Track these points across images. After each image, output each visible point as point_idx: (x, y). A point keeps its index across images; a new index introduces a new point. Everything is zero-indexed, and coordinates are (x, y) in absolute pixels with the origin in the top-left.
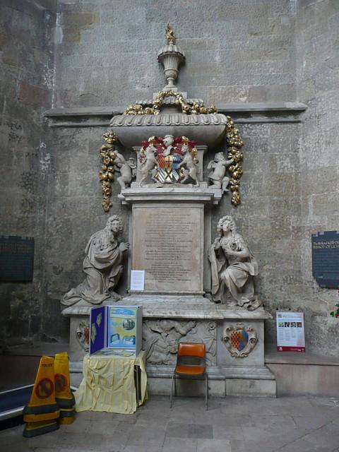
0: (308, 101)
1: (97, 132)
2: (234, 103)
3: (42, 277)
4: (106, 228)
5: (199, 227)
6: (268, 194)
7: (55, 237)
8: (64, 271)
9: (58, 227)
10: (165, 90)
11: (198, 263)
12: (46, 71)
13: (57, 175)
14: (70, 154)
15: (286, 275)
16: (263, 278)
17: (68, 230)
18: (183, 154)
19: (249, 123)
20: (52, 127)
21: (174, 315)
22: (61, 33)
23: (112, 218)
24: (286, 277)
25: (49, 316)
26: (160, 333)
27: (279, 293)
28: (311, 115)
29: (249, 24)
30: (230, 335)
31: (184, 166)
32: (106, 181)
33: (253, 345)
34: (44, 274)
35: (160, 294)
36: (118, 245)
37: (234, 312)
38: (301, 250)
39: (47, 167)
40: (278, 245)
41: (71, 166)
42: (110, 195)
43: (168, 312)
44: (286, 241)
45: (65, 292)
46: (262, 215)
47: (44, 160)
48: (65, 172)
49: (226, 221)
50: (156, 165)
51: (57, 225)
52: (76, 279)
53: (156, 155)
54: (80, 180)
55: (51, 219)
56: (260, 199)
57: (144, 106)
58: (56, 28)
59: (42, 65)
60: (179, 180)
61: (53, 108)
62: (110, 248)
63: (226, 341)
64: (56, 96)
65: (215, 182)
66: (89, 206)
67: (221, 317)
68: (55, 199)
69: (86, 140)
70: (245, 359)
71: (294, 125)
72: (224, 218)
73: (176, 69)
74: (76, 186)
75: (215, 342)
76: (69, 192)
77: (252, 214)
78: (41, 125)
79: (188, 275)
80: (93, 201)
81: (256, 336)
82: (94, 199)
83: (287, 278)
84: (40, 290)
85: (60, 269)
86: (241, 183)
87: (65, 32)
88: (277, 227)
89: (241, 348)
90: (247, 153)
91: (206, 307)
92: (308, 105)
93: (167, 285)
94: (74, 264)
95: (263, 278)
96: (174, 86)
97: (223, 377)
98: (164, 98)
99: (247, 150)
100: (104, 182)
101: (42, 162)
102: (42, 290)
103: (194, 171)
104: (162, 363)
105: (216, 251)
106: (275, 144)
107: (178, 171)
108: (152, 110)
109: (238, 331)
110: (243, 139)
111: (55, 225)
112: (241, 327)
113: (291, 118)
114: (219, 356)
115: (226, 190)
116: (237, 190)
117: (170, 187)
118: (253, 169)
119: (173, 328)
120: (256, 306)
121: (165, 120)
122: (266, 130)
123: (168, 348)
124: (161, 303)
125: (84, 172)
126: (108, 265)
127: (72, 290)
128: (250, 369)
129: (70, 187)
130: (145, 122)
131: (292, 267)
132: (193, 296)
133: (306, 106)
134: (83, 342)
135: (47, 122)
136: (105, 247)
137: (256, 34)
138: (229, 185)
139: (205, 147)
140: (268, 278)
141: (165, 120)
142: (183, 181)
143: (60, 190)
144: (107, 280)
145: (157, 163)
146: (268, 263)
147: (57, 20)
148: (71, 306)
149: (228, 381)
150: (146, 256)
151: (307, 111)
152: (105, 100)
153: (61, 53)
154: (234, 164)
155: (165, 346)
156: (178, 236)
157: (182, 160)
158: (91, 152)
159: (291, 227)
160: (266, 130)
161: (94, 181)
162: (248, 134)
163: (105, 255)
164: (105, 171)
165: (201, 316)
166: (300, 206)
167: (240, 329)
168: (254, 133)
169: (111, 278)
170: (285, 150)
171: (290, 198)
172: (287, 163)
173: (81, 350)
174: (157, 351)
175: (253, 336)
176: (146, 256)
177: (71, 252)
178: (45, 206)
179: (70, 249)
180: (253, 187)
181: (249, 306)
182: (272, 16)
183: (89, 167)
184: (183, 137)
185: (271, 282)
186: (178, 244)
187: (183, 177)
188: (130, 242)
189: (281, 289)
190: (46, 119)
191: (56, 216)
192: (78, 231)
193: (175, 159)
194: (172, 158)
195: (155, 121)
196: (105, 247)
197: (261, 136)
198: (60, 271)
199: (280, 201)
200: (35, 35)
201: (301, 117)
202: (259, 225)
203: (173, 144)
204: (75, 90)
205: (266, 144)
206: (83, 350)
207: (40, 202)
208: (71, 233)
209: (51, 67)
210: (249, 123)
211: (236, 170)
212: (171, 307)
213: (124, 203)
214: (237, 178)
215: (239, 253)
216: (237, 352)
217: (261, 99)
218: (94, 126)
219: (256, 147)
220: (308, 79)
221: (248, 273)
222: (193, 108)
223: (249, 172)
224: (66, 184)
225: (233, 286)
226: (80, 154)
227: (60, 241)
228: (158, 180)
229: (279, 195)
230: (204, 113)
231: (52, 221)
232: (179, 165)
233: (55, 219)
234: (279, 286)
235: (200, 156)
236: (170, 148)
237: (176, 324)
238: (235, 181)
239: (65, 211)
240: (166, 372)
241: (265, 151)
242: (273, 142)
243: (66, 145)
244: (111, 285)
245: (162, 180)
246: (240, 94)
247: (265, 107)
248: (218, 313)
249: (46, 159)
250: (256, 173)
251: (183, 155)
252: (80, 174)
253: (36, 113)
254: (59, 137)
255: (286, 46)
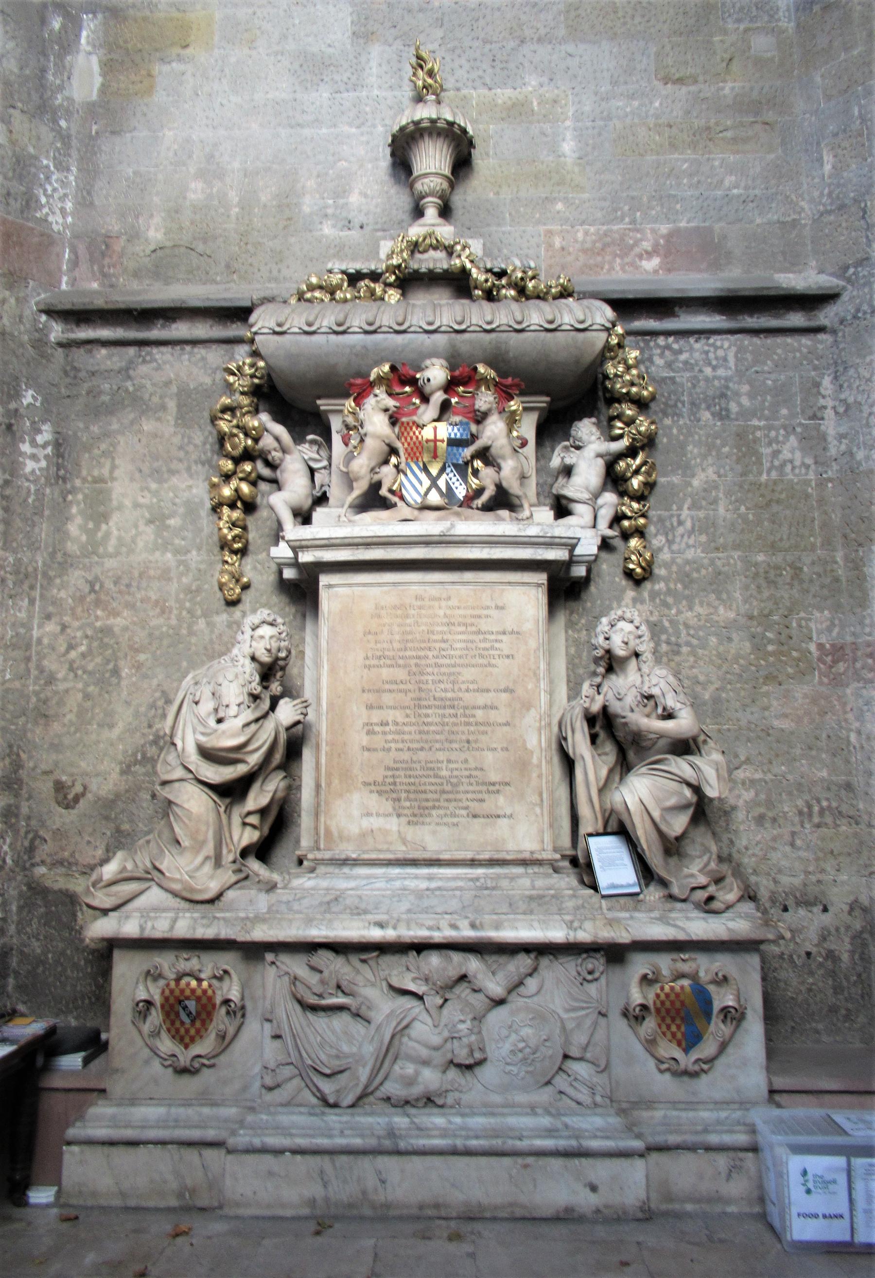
0: (847, 268)
1: (203, 359)
2: (622, 276)
3: (17, 816)
4: (235, 651)
5: (533, 644)
6: (736, 547)
7: (61, 687)
8: (89, 796)
9: (73, 654)
10: (416, 231)
11: (535, 761)
12: (48, 178)
13: (73, 491)
14: (115, 426)
15: (807, 797)
16: (734, 808)
17: (108, 661)
18: (480, 418)
19: (667, 333)
20: (61, 345)
21: (467, 933)
22: (96, 68)
23: (255, 619)
24: (807, 802)
25: (36, 947)
26: (420, 998)
27: (785, 856)
28: (858, 310)
29: (658, 54)
30: (651, 996)
31: (484, 454)
32: (232, 506)
33: (725, 1030)
34: (24, 810)
35: (414, 863)
36: (273, 707)
37: (663, 920)
38: (850, 716)
39: (44, 464)
40: (775, 703)
41: (117, 462)
42: (243, 552)
43: (444, 924)
44: (801, 692)
45: (92, 868)
46: (721, 610)
47: (33, 443)
48: (100, 480)
49: (622, 624)
50: (393, 451)
51: (71, 647)
52: (131, 821)
53: (394, 421)
54: (149, 507)
55: (51, 627)
56: (712, 562)
57: (354, 278)
58: (81, 58)
59: (36, 158)
60: (468, 501)
61: (64, 287)
62: (248, 715)
63: (639, 1019)
64: (74, 251)
65: (578, 508)
66: (174, 586)
67: (623, 937)
68: (66, 564)
69: (168, 383)
70: (704, 1078)
71: (806, 341)
72: (613, 615)
73: (447, 171)
74: (136, 526)
75: (602, 1021)
76: (113, 542)
77: (691, 609)
78: (26, 338)
79: (501, 800)
80: (188, 569)
81: (738, 999)
82: (193, 566)
83: (810, 807)
84: (9, 861)
85: (78, 789)
86: (651, 513)
87: (109, 67)
88: (770, 648)
89: (691, 1041)
90: (668, 422)
91: (570, 904)
92: (849, 280)
93: (434, 833)
94: (123, 772)
95: (734, 808)
96: (440, 221)
97: (637, 1144)
98: (413, 252)
99: (665, 414)
100: (226, 510)
101: (26, 448)
102: (16, 862)
103: (515, 469)
104: (429, 1101)
105: (591, 720)
106: (752, 396)
107: (462, 469)
108: (378, 288)
109: (677, 985)
110: (653, 380)
111: (63, 649)
112: (686, 968)
113: (796, 319)
114: (618, 1070)
115: (610, 533)
116: (640, 532)
117: (439, 519)
118: (687, 470)
119: (463, 978)
120: (731, 897)
121: (418, 319)
122: (720, 353)
123: (448, 1045)
124: (419, 895)
125: (161, 481)
126: (241, 769)
127: (120, 855)
128: (723, 1114)
129: (115, 526)
130: (357, 321)
131: (824, 774)
132: (520, 870)
133: (842, 283)
134: (155, 1034)
135: (46, 328)
136: (233, 710)
137: (680, 81)
138: (617, 519)
139: (542, 401)
140: (751, 805)
141: (418, 319)
142: (479, 502)
143: (84, 538)
144: (236, 820)
145: (398, 445)
146: (748, 761)
147: (84, 34)
148: (115, 909)
149: (654, 1156)
150: (365, 740)
151: (845, 297)
152: (228, 266)
153: (95, 128)
154: (631, 452)
155: (436, 1040)
156: (468, 674)
157: (474, 438)
158: (183, 419)
159: (813, 647)
160: (720, 353)
161: (191, 510)
162: (669, 365)
163: (234, 736)
164: (227, 477)
165: (557, 934)
166: (837, 580)
167: (683, 976)
168: (686, 363)
169: (249, 813)
170: (784, 412)
171: (807, 559)
172: (792, 452)
173: (147, 1062)
174: (410, 1058)
175: (730, 1002)
176: (365, 740)
177: (116, 732)
178: (32, 587)
179: (111, 726)
180: (689, 524)
181: (711, 898)
182: (725, 32)
183: (175, 465)
184: (482, 369)
185: (760, 820)
186: (469, 698)
187: (480, 492)
188: (308, 693)
189: (792, 845)
190: (44, 318)
191: (67, 619)
192: (138, 666)
193: (456, 433)
194: (444, 431)
195: (386, 319)
196: (233, 710)
197: (708, 371)
198: (77, 799)
199: (777, 567)
200: (16, 70)
201: (826, 316)
202: (713, 640)
203: (449, 387)
204: (134, 236)
205: (723, 395)
206: (156, 1064)
207: (17, 572)
208: (116, 672)
209: (61, 167)
210: (667, 333)
211: (637, 472)
212: (454, 905)
213: (289, 574)
214: (640, 498)
215: (669, 725)
216: (678, 1054)
217: (703, 266)
218: (194, 342)
219: (693, 404)
220: (842, 207)
221: (697, 790)
222: (504, 281)
223: (676, 479)
224: (105, 517)
225: (654, 835)
226: (148, 426)
227: (80, 696)
228: (402, 498)
229: (773, 548)
230: (538, 297)
231: (55, 636)
232: (468, 452)
233: (64, 627)
234: (786, 831)
235: (528, 428)
236: (438, 397)
237: (473, 964)
238: (635, 505)
239: (98, 603)
240: (444, 1133)
241: (723, 415)
242: (745, 388)
243: (106, 398)
244: (250, 836)
245: (413, 496)
246: (637, 250)
247: (719, 285)
248: (610, 923)
249: (40, 439)
250: (696, 483)
251: (478, 422)
252: (148, 489)
253: (13, 301)
254: (83, 374)
255: (770, 116)
